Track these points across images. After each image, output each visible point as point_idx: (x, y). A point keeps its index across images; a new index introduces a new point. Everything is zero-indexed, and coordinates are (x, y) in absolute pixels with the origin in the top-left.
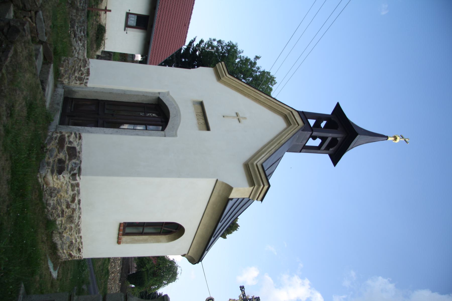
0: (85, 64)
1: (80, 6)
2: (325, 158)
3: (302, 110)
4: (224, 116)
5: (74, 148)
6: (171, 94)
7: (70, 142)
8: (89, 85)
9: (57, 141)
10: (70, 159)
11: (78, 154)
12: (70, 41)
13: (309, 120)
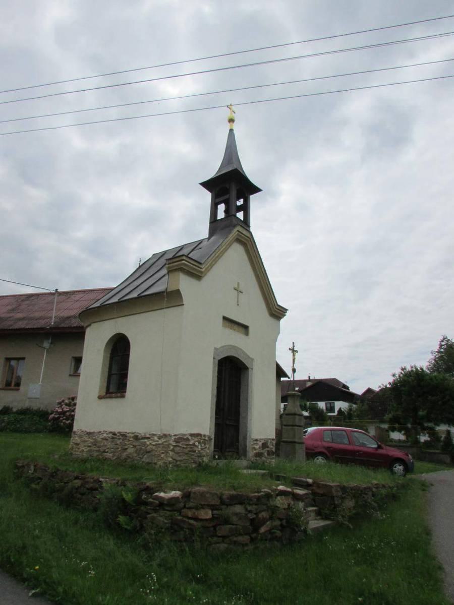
0: (184, 439)
1: (194, 503)
2: (254, 199)
3: (209, 225)
4: (238, 305)
5: (263, 444)
6: (218, 347)
7: (259, 448)
8: (207, 433)
9: (258, 458)
10: (268, 447)
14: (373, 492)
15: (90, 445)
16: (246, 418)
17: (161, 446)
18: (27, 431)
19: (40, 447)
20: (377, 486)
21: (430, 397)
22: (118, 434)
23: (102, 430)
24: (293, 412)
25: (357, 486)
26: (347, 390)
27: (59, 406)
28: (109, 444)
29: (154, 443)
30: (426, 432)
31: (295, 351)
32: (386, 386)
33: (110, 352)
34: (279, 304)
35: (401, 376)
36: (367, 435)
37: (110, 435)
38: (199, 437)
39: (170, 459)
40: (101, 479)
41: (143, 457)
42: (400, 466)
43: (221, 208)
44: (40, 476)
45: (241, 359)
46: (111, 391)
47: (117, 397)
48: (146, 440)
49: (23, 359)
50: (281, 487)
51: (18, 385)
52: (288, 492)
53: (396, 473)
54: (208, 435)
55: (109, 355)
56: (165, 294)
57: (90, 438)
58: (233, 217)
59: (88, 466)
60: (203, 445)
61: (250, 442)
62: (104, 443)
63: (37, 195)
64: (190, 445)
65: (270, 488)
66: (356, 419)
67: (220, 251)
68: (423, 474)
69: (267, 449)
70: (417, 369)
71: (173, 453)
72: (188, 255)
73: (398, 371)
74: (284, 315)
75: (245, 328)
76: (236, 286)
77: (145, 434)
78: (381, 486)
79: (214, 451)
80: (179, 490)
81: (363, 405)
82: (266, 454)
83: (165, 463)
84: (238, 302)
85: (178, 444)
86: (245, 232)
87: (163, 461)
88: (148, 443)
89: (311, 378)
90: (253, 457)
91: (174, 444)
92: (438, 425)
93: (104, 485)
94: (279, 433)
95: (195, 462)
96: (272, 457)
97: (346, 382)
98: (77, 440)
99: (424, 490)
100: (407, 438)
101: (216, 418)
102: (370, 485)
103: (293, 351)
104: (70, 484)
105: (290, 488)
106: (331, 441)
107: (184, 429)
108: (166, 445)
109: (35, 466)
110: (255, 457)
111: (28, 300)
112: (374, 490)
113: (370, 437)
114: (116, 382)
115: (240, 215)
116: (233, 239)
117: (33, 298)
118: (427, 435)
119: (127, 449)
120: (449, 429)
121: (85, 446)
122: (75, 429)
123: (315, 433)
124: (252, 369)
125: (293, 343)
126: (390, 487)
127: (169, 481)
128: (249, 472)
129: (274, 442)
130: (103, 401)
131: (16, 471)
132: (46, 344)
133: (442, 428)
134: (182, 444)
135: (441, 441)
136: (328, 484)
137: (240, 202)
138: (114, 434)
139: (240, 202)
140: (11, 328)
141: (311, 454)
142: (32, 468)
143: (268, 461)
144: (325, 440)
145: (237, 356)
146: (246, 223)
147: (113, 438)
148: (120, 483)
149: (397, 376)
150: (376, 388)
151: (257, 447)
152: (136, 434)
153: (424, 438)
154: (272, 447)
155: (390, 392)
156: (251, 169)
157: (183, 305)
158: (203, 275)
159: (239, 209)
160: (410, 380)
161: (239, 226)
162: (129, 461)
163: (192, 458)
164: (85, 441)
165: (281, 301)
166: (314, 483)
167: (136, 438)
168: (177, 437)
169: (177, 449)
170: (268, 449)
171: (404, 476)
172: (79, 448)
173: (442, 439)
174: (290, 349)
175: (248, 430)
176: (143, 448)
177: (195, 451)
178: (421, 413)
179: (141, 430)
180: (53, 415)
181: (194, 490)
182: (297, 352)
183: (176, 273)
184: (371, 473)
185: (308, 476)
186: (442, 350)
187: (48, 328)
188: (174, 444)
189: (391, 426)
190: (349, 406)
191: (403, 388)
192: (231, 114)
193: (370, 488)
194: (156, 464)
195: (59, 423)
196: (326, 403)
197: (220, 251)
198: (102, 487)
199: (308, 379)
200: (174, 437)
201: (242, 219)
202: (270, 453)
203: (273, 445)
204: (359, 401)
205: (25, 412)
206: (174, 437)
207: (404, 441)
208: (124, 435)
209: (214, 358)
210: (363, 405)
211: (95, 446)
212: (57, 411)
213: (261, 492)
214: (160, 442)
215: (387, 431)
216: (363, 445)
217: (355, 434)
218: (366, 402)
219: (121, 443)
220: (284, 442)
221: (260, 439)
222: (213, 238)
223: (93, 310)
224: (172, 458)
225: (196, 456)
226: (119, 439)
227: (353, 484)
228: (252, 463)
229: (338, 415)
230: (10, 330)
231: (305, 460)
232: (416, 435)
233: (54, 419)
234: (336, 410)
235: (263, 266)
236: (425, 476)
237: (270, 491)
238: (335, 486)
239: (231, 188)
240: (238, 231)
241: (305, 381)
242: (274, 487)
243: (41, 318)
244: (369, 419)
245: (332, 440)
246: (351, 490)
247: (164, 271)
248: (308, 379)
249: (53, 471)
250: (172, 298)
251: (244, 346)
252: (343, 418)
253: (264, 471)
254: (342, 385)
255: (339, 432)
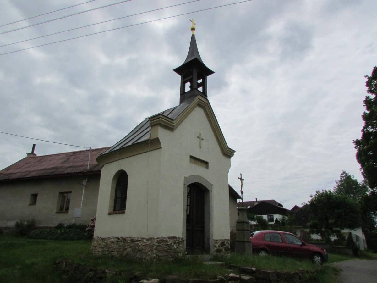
2: (209, 78)
4: (200, 148)
6: (187, 176)
7: (219, 246)
8: (181, 236)
9: (218, 253)
10: (225, 245)
11: (223, 241)
12: (253, 276)
13: (198, 89)
14: (299, 276)
15: (103, 247)
16: (209, 225)
17: (149, 246)
18: (72, 239)
19: (72, 250)
20: (302, 272)
21: (336, 210)
22: (121, 239)
23: (111, 236)
24: (243, 221)
25: (287, 272)
26: (281, 207)
27: (92, 222)
28: (115, 246)
29: (144, 244)
30: (335, 234)
31: (243, 179)
32: (307, 204)
33: (116, 183)
34: (229, 147)
35: (316, 196)
36: (295, 236)
37: (116, 240)
38: (175, 239)
39: (154, 255)
40: (106, 271)
41: (137, 254)
42: (318, 257)
43: (188, 85)
44: (69, 270)
45: (204, 185)
46: (116, 209)
47: (120, 213)
48: (138, 242)
49: (71, 192)
50: (232, 275)
51: (67, 209)
52: (237, 278)
53: (315, 262)
54: (181, 238)
55: (115, 185)
56: (149, 141)
57: (103, 242)
58: (195, 90)
59: (100, 261)
60: (178, 245)
61: (212, 242)
62: (112, 245)
63: (81, 93)
64: (168, 245)
65: (223, 276)
66: (288, 226)
67: (186, 113)
68: (335, 263)
69: (224, 247)
70: (326, 192)
71: (156, 251)
72: (168, 115)
73: (314, 194)
74: (234, 155)
75: (206, 164)
76: (199, 135)
77: (138, 238)
78: (305, 272)
79: (186, 249)
80: (157, 278)
81: (292, 217)
82: (224, 250)
83: (151, 258)
84: (200, 146)
85: (160, 244)
86: (203, 99)
87: (149, 257)
88: (140, 244)
89: (257, 200)
90: (214, 252)
91: (157, 244)
92: (343, 229)
93: (107, 275)
94: (232, 234)
95: (172, 257)
96: (228, 252)
97: (280, 202)
98: (95, 244)
99: (336, 274)
100: (322, 237)
101: (187, 226)
102: (297, 271)
103: (241, 179)
104: (87, 274)
105: (238, 275)
106: (270, 240)
107: (164, 234)
108: (152, 245)
109: (66, 263)
110: (216, 252)
111: (74, 155)
112: (300, 274)
113: (297, 237)
114: (119, 204)
115: (201, 89)
116: (195, 104)
117: (77, 154)
118: (336, 236)
119: (126, 249)
120: (350, 231)
121: (100, 248)
122: (95, 235)
123: (259, 235)
124: (212, 191)
125: (241, 174)
126: (311, 272)
127: (152, 271)
128: (210, 263)
129: (229, 242)
130: (111, 215)
131: (55, 266)
132: (84, 183)
133: (346, 231)
134: (163, 244)
135: (346, 240)
136: (267, 271)
137: (200, 81)
138: (118, 238)
139: (200, 81)
140: (62, 173)
141: (257, 249)
142: (64, 264)
143: (225, 255)
144: (266, 240)
145: (200, 182)
146: (204, 94)
147: (117, 242)
148: (118, 274)
149: (314, 196)
150: (300, 206)
151: (217, 245)
152: (132, 238)
153: (333, 238)
154: (227, 245)
155: (310, 207)
156: (208, 61)
157: (161, 148)
158: (175, 128)
159: (199, 85)
160: (322, 199)
161: (199, 96)
162: (127, 257)
163: (170, 254)
164: (100, 244)
165: (230, 145)
166: (257, 270)
167: (132, 241)
168: (159, 239)
169: (159, 248)
170: (226, 247)
171: (322, 264)
172: (96, 249)
173: (346, 238)
174: (239, 178)
175: (211, 233)
176: (137, 247)
177: (172, 249)
178: (331, 221)
179: (135, 236)
180: (88, 228)
181: (168, 277)
182: (244, 180)
183: (156, 127)
184: (298, 263)
185: (253, 266)
186: (343, 180)
187: (85, 172)
188: (157, 244)
189: (311, 230)
190: (282, 217)
191: (318, 205)
192: (193, 25)
193: (297, 274)
194: (145, 259)
195: (84, 232)
196: (268, 216)
197: (186, 113)
198: (106, 277)
199: (255, 200)
200: (157, 240)
201: (202, 91)
202: (227, 249)
203: (228, 244)
204: (289, 214)
205: (71, 227)
206: (157, 240)
207: (320, 240)
208: (124, 239)
209: (184, 184)
210: (292, 217)
211: (106, 248)
212: (90, 226)
213: (217, 278)
214: (148, 243)
215: (309, 234)
216: (292, 243)
217: (287, 236)
218: (294, 214)
219: (122, 245)
220: (237, 241)
221: (219, 240)
222: (182, 104)
223: (105, 155)
224: (155, 254)
225: (173, 253)
226: (122, 242)
227: (286, 271)
228: (215, 257)
229: (275, 223)
230: (62, 174)
231: (252, 254)
232: (329, 236)
233: (89, 230)
234: (275, 219)
235: (217, 122)
236: (335, 264)
237: (223, 278)
238: (272, 273)
239: (193, 71)
240: (199, 99)
241: (254, 202)
242: (226, 274)
243: (81, 166)
244: (297, 226)
245: (271, 240)
246: (284, 275)
247: (150, 128)
248: (255, 200)
249: (77, 266)
250: (154, 144)
251: (205, 175)
252: (279, 225)
253: (222, 263)
254: (278, 204)
255: (275, 234)
